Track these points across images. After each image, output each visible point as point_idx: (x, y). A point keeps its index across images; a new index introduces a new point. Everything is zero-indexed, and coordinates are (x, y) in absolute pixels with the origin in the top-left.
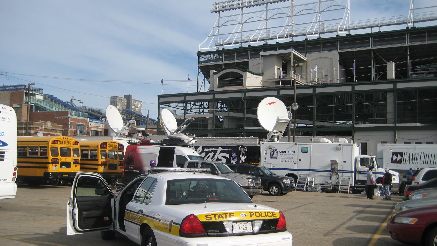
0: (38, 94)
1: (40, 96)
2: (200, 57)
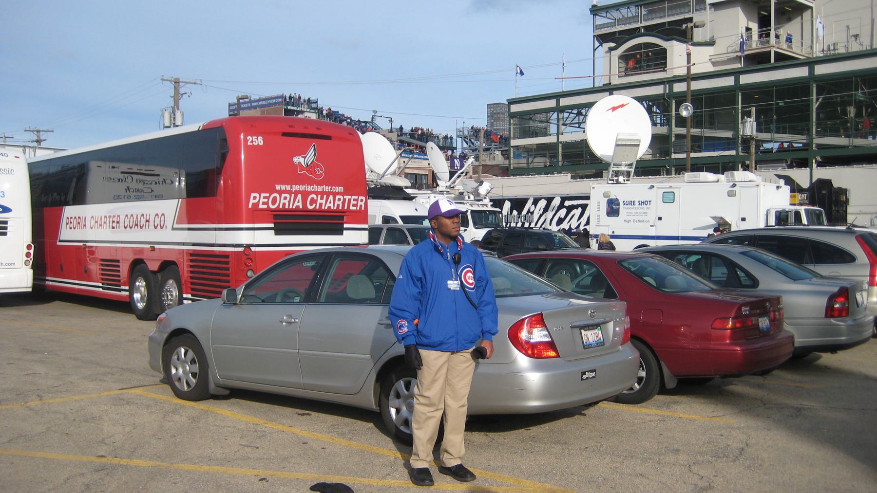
0: (308, 110)
1: (312, 114)
2: (597, 16)
